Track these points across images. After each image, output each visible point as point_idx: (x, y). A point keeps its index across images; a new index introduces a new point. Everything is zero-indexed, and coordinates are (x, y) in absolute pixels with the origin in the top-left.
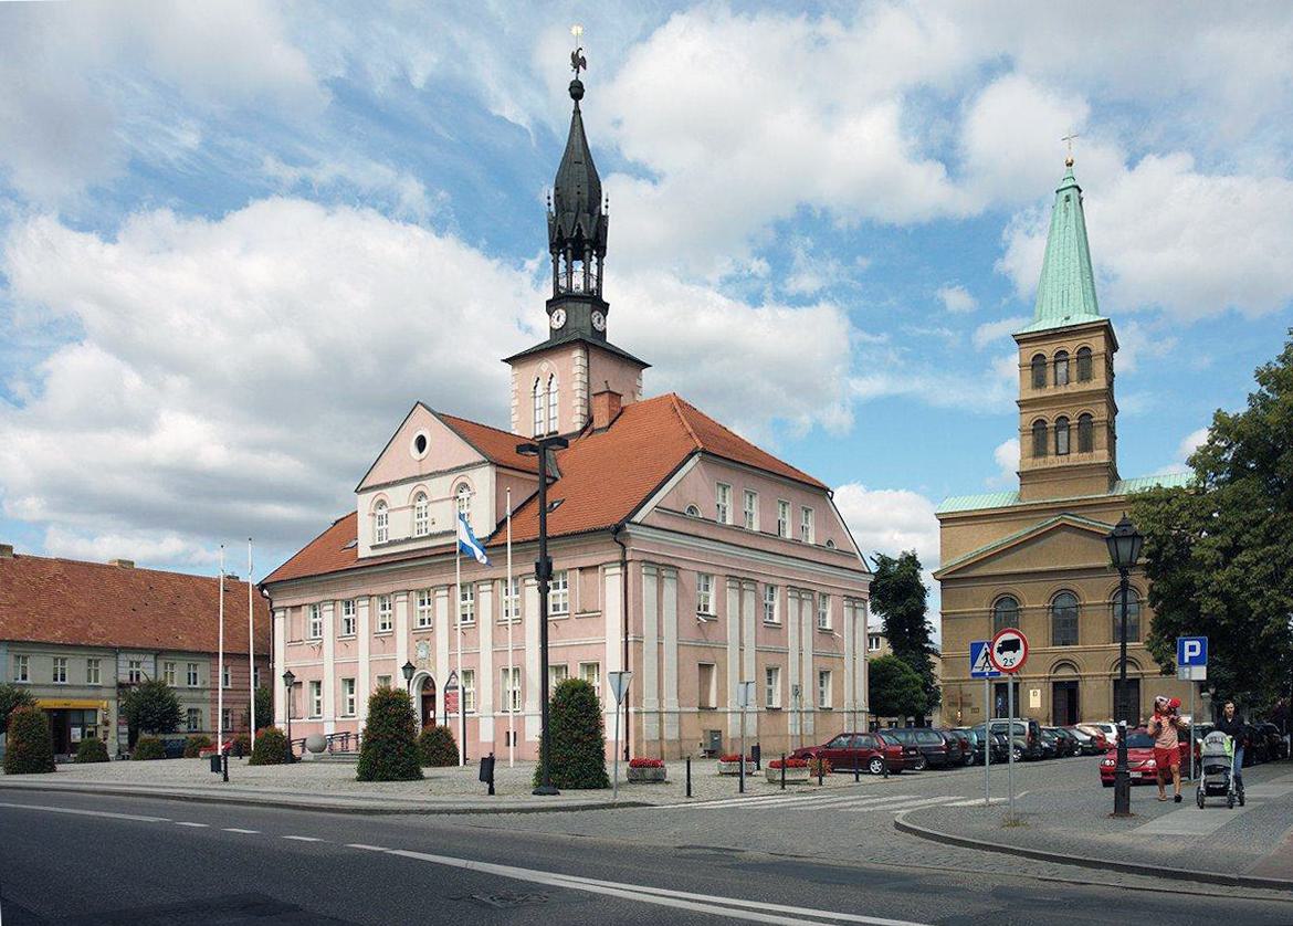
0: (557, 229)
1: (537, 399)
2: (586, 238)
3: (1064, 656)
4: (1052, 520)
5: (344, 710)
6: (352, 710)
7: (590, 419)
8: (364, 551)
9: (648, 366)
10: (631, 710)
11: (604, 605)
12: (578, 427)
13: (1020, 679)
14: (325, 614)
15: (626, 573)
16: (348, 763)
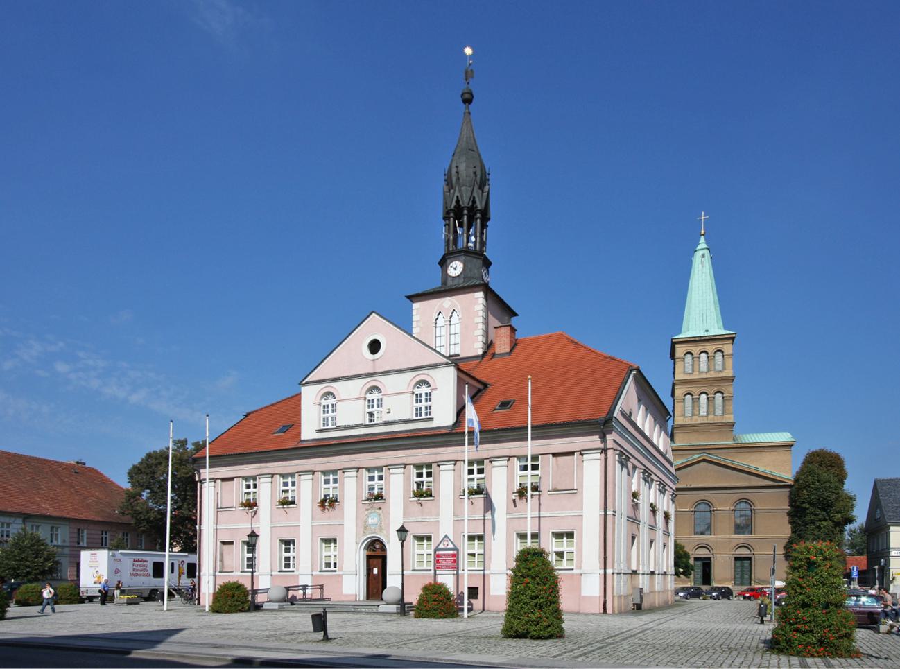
0: (455, 198)
1: (437, 329)
2: (479, 208)
3: (702, 542)
4: (696, 456)
5: (280, 566)
6: (287, 566)
7: (489, 345)
8: (308, 432)
9: (516, 315)
10: (609, 571)
11: (581, 483)
12: (480, 352)
13: (713, 555)
14: (346, 480)
15: (606, 459)
16: (302, 612)
